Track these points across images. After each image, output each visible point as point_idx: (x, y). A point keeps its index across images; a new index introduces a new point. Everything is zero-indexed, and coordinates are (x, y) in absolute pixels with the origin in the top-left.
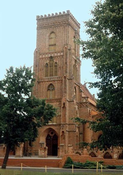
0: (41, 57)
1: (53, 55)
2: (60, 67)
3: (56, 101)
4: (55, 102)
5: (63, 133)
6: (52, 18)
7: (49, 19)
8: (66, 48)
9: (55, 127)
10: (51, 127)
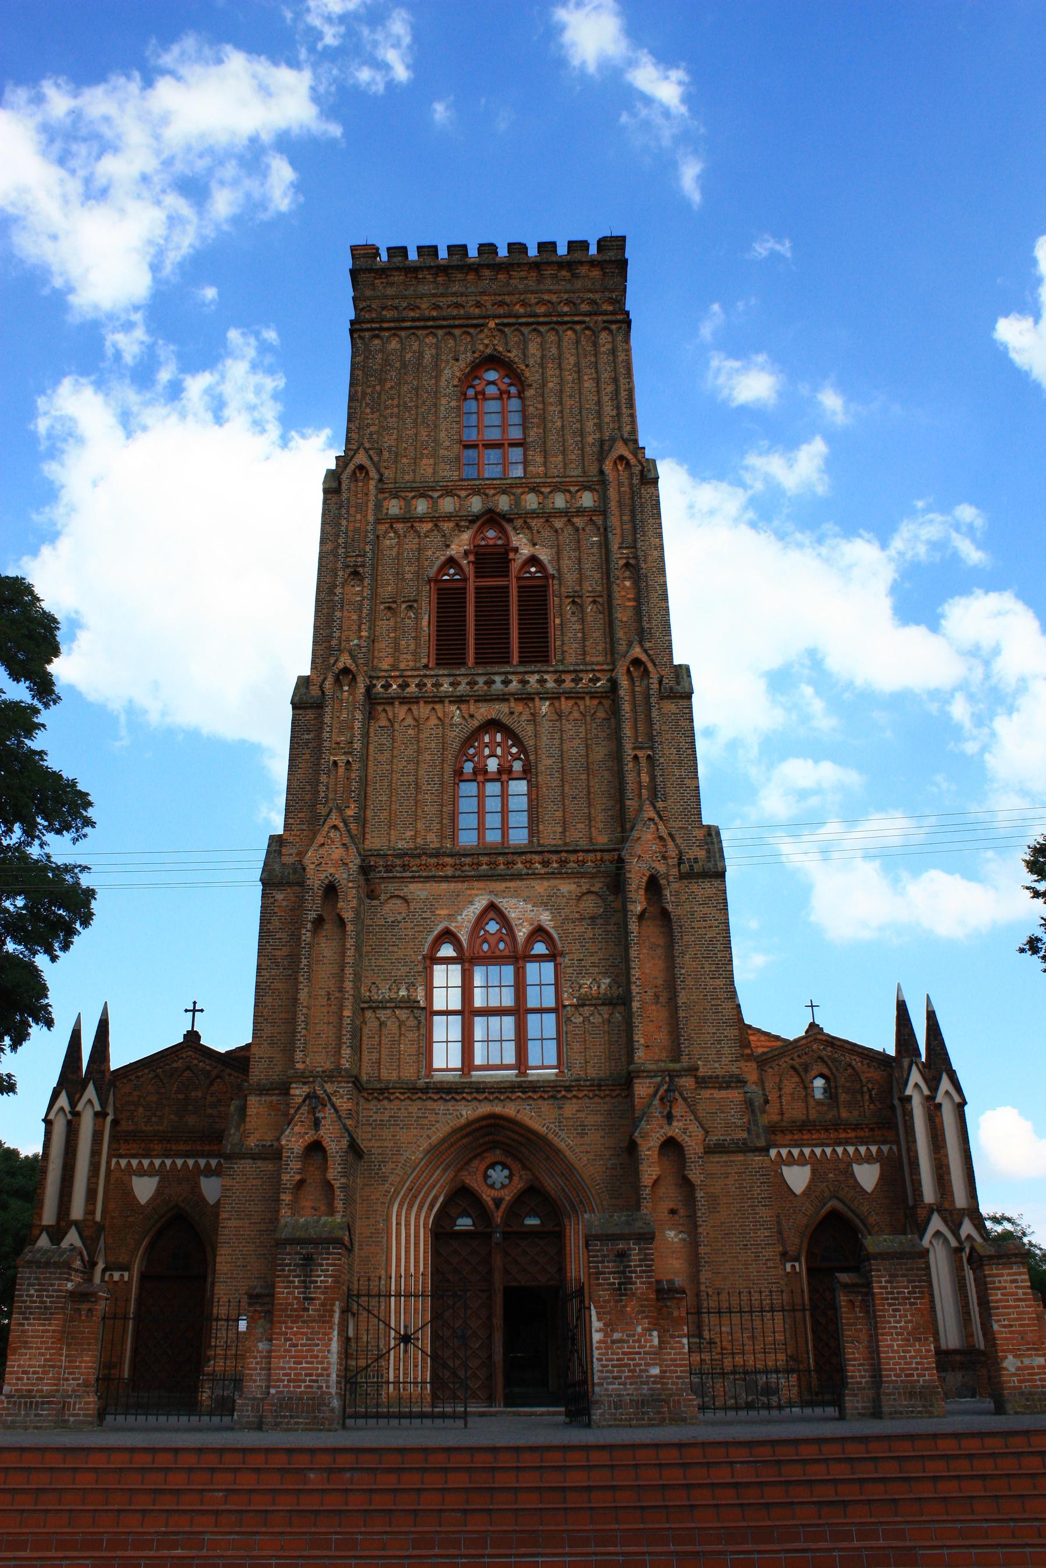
0: (394, 507)
1: (503, 503)
2: (575, 599)
3: (545, 863)
4: (542, 877)
5: (91, 1207)
6: (487, 273)
7: (460, 276)
8: (621, 458)
9: (545, 1106)
10: (509, 1110)
